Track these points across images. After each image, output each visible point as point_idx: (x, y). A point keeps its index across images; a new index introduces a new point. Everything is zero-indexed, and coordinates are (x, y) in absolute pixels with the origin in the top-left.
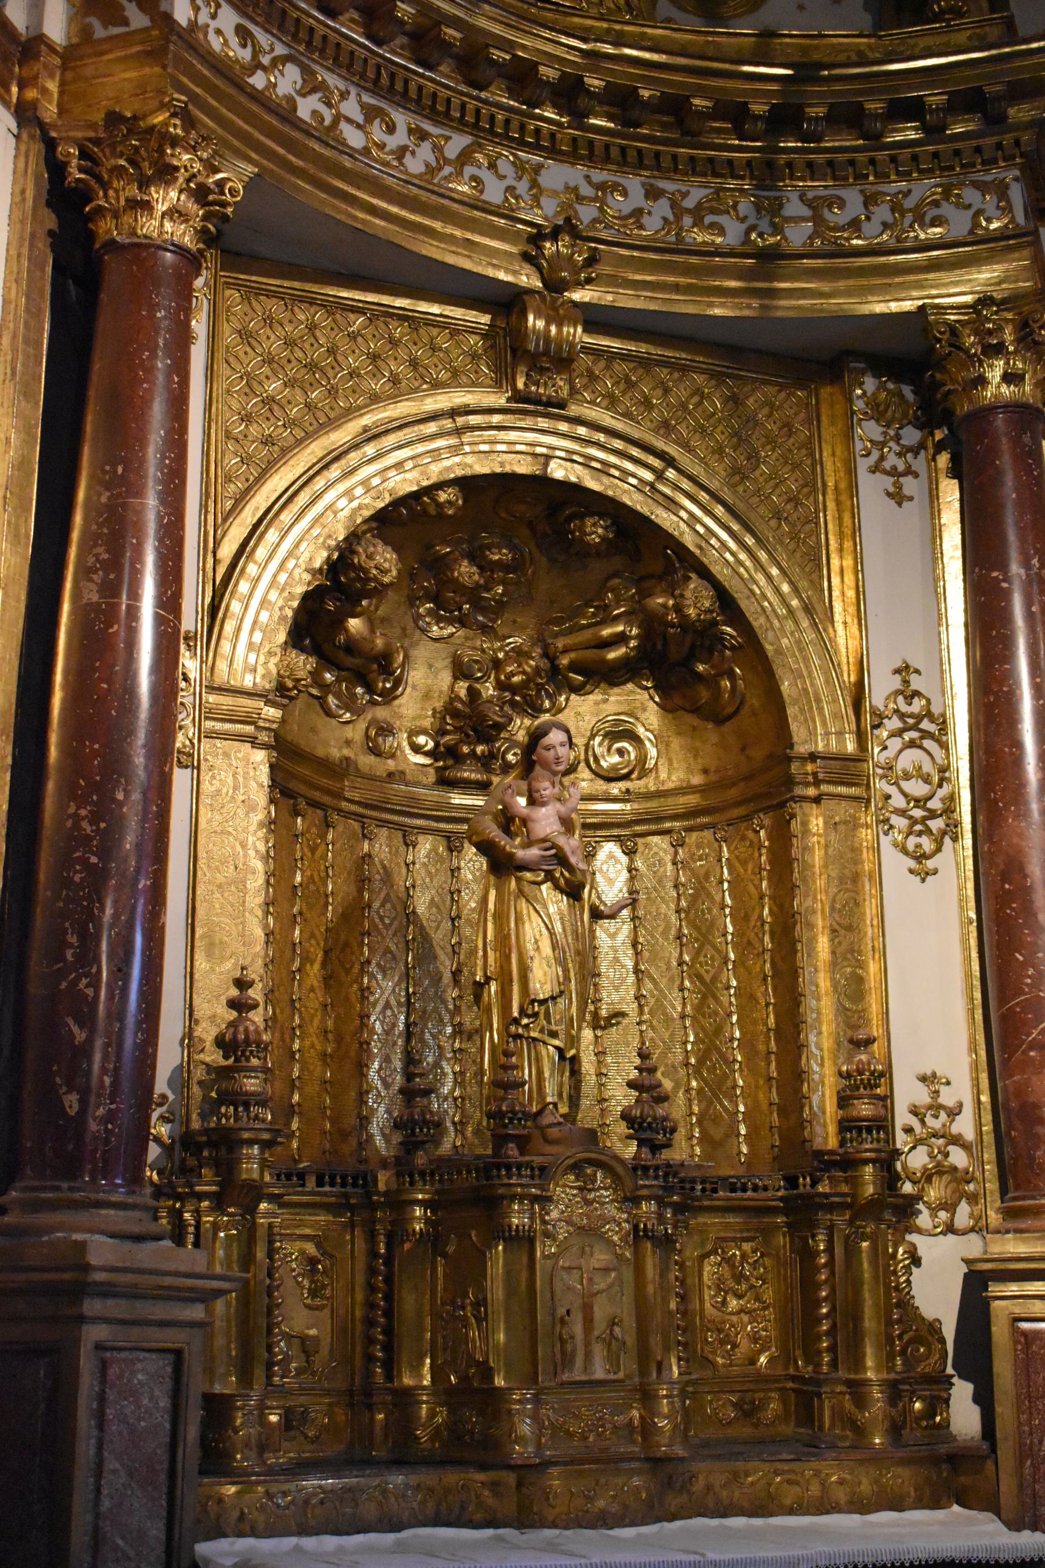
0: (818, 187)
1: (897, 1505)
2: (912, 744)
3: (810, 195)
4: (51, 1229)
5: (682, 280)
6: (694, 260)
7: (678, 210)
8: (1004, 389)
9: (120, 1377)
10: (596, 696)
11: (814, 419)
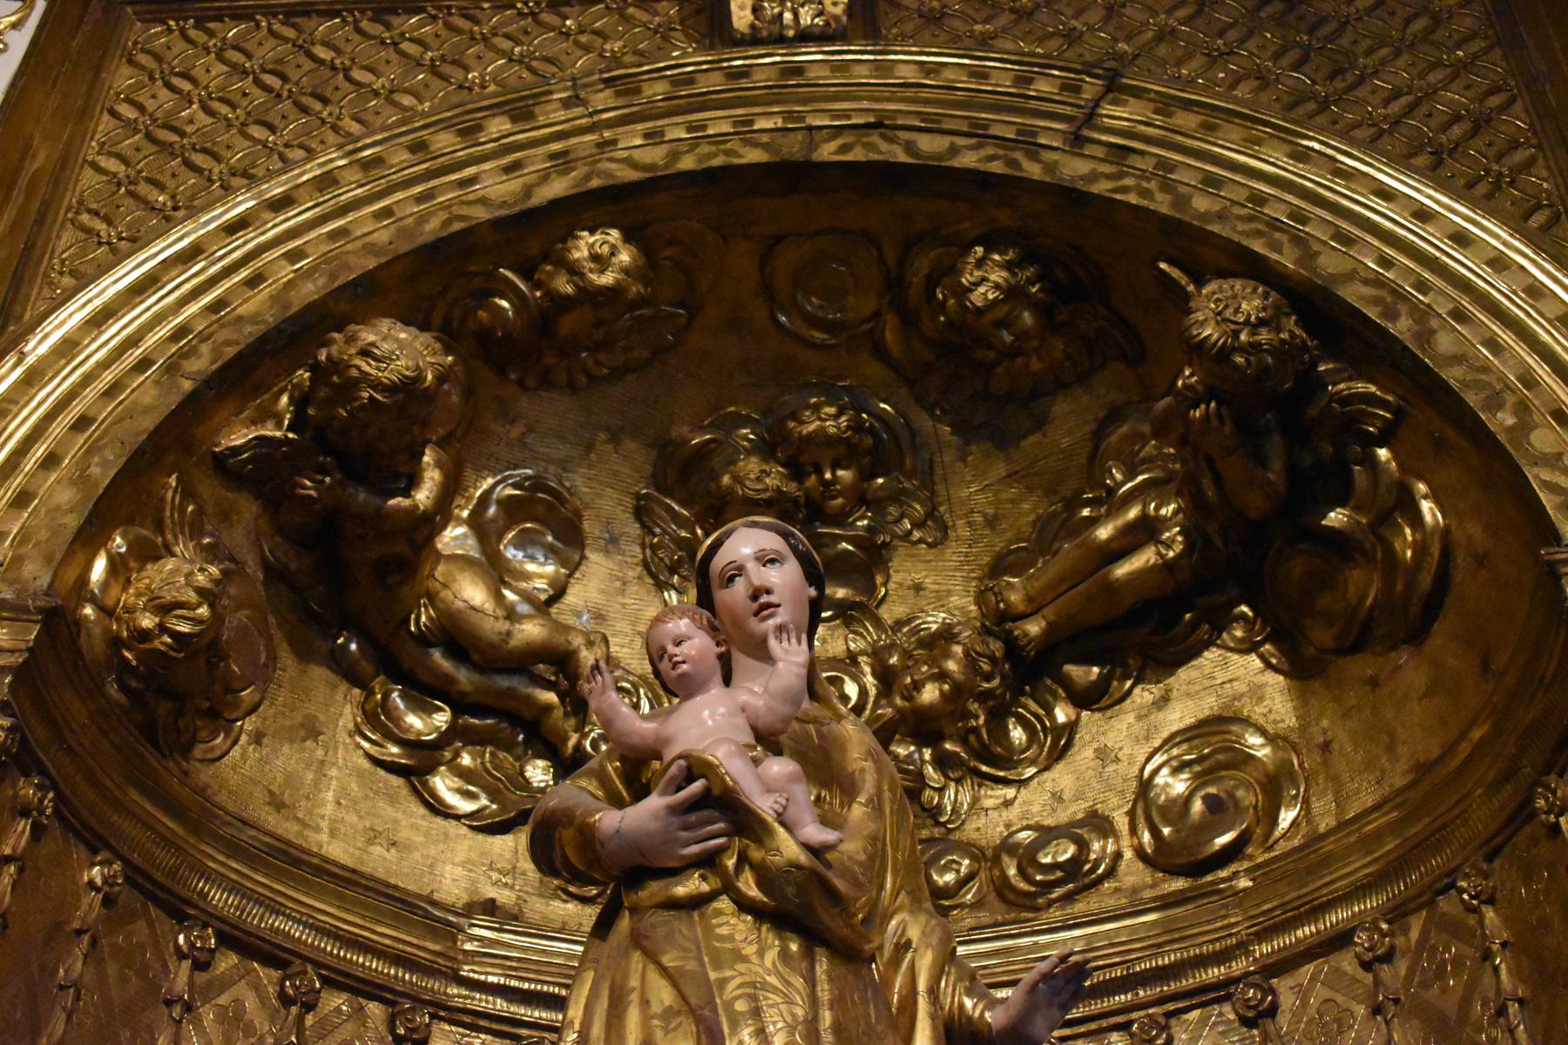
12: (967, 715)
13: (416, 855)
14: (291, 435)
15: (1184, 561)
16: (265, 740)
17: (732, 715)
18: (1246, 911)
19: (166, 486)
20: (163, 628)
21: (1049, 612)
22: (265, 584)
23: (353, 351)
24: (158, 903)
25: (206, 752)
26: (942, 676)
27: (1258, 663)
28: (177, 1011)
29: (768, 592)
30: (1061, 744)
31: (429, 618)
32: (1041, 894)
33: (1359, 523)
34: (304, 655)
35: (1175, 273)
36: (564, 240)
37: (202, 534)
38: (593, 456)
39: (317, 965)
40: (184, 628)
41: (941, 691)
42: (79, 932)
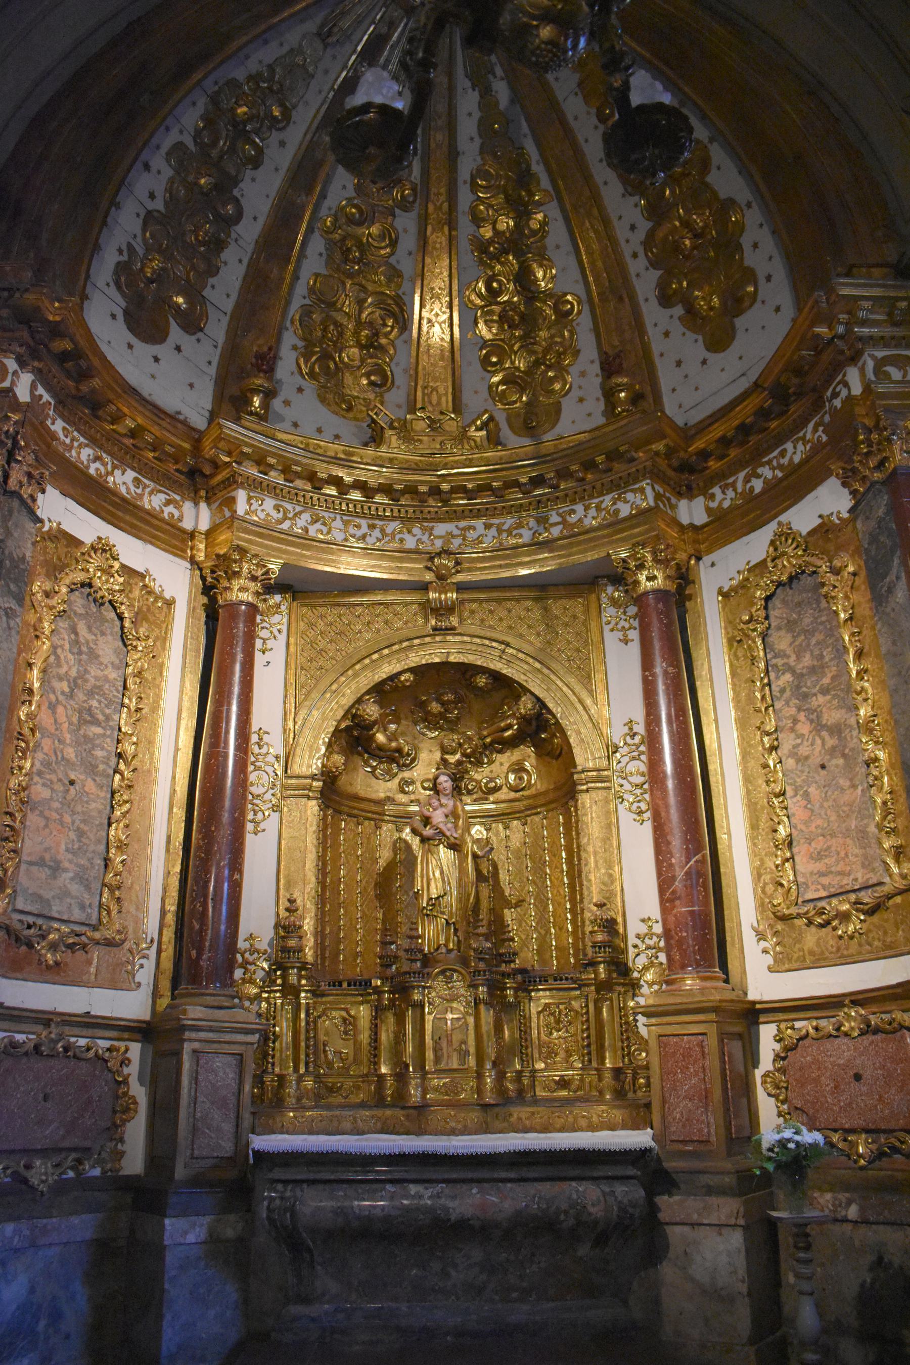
0: (564, 508)
1: (612, 1128)
2: (634, 758)
3: (561, 511)
4: (182, 1005)
5: (502, 562)
6: (508, 552)
7: (500, 531)
8: (648, 584)
9: (207, 1063)
10: (508, 754)
11: (587, 611)
30: (491, 762)
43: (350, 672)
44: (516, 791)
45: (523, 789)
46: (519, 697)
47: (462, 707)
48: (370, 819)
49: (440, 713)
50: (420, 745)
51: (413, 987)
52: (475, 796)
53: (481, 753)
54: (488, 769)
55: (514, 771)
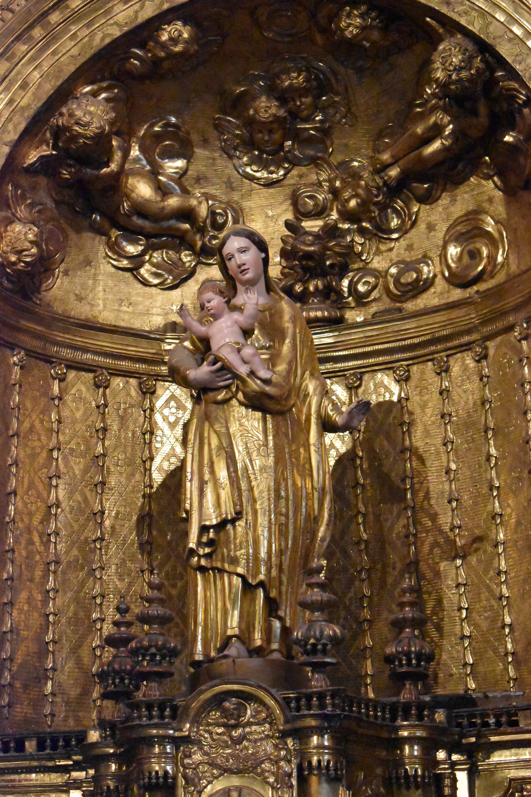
10: (445, 200)
12: (370, 211)
13: (141, 307)
14: (54, 153)
15: (454, 146)
16: (70, 273)
17: (232, 326)
18: (477, 312)
19: (7, 190)
20: (20, 260)
21: (401, 163)
22: (57, 208)
23: (72, 122)
24: (40, 359)
25: (47, 286)
26: (356, 196)
27: (492, 185)
28: (56, 402)
29: (244, 264)
30: (408, 225)
31: (128, 206)
32: (404, 296)
33: (519, 139)
34: (78, 231)
35: (433, 23)
36: (157, 31)
37: (26, 199)
38: (191, 105)
39: (106, 369)
40: (28, 259)
41: (357, 202)
42: (14, 385)
43: (37, 32)
44: (465, 285)
45: (479, 278)
46: (434, 41)
47: (333, 104)
48: (127, 374)
49: (277, 119)
50: (246, 204)
51: (150, 741)
52: (374, 308)
53: (383, 207)
54: (403, 243)
55: (459, 239)
